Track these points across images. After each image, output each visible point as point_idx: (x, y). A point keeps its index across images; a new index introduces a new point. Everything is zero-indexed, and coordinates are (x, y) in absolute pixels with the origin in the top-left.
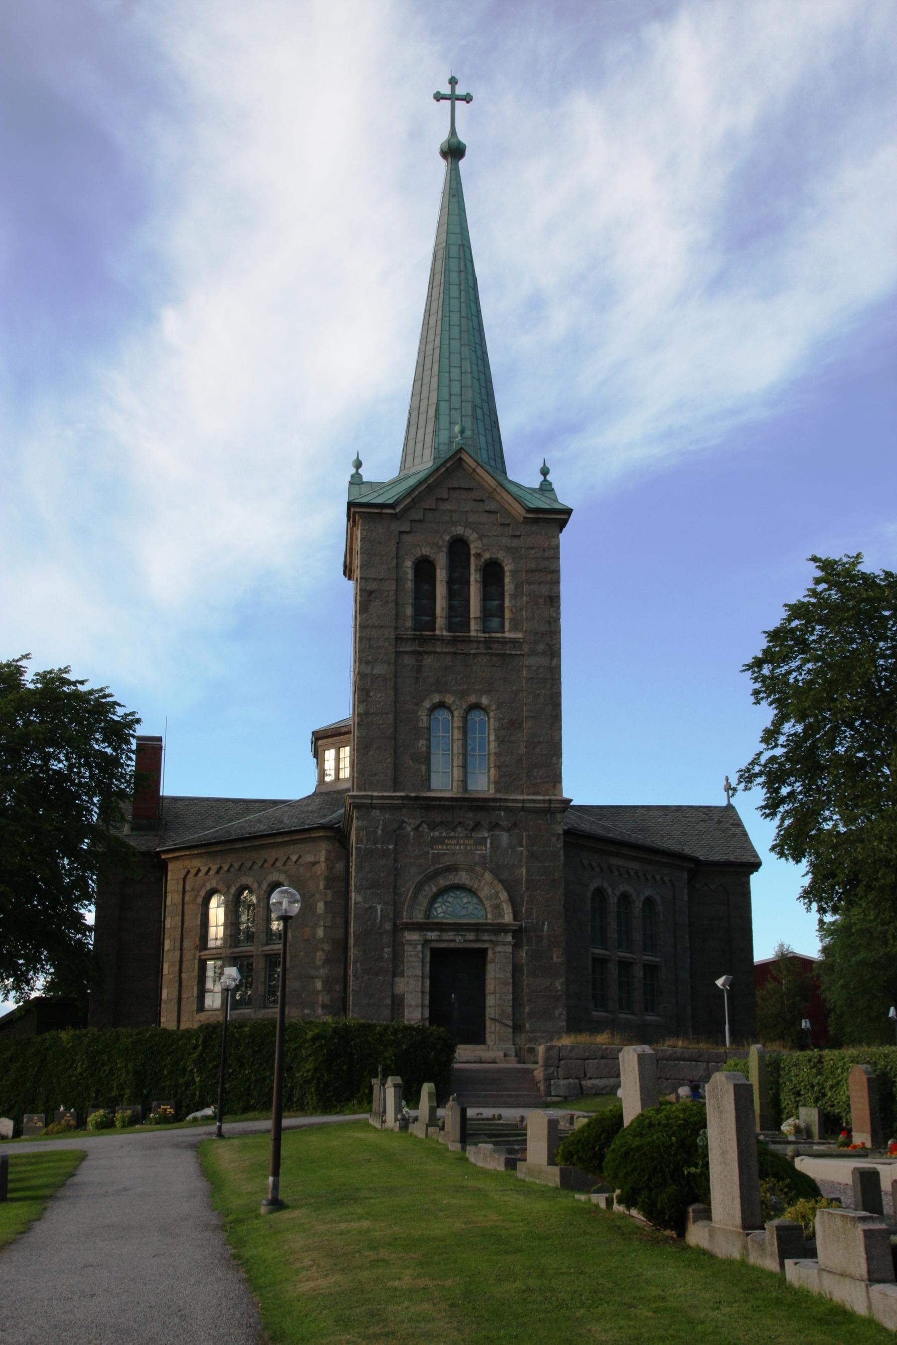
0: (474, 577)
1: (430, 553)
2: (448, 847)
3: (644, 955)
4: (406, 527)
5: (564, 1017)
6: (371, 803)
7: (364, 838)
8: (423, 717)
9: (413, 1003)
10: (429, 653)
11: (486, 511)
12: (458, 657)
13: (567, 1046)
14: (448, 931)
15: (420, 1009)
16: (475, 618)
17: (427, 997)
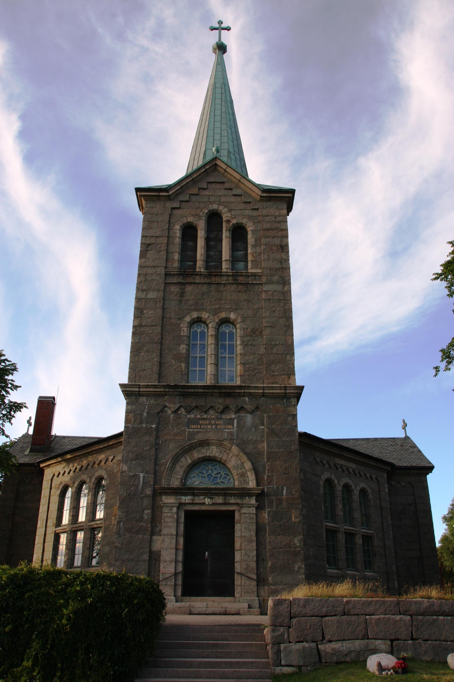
0: (226, 237)
1: (193, 220)
2: (202, 427)
3: (362, 529)
4: (176, 205)
5: (302, 571)
6: (139, 391)
7: (132, 418)
8: (183, 328)
9: (168, 558)
10: (190, 283)
11: (234, 195)
12: (213, 286)
13: (299, 599)
14: (200, 496)
15: (174, 565)
16: (226, 260)
17: (181, 554)
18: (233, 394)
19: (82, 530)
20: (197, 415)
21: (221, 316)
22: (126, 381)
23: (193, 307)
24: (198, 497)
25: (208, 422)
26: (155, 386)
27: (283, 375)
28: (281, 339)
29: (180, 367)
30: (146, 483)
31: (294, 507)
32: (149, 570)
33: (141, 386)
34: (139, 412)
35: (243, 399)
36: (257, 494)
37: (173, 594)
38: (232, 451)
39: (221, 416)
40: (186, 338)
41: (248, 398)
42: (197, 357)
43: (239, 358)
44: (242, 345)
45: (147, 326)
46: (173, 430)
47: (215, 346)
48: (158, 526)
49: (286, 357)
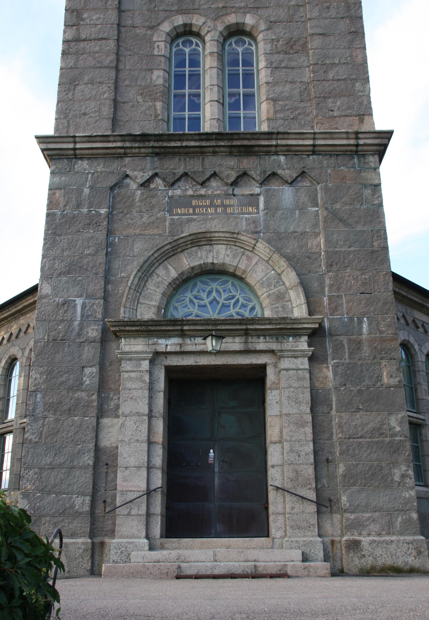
2: (197, 211)
7: (62, 199)
14: (195, 337)
18: (257, 149)
19: (11, 432)
20: (186, 190)
21: (229, 21)
22: (50, 131)
23: (175, 8)
24: (192, 339)
25: (208, 202)
26: (105, 138)
27: (350, 116)
28: (343, 55)
29: (153, 107)
30: (88, 317)
31: (385, 355)
32: (94, 486)
33: (77, 139)
34: (75, 187)
35: (275, 160)
36: (310, 331)
37: (144, 534)
38: (256, 252)
39: (233, 190)
40: (163, 59)
41: (284, 157)
42: (185, 95)
43: (263, 90)
44: (268, 68)
45: (90, 40)
46: (142, 218)
47: (218, 72)
48: (112, 399)
49: (354, 85)
